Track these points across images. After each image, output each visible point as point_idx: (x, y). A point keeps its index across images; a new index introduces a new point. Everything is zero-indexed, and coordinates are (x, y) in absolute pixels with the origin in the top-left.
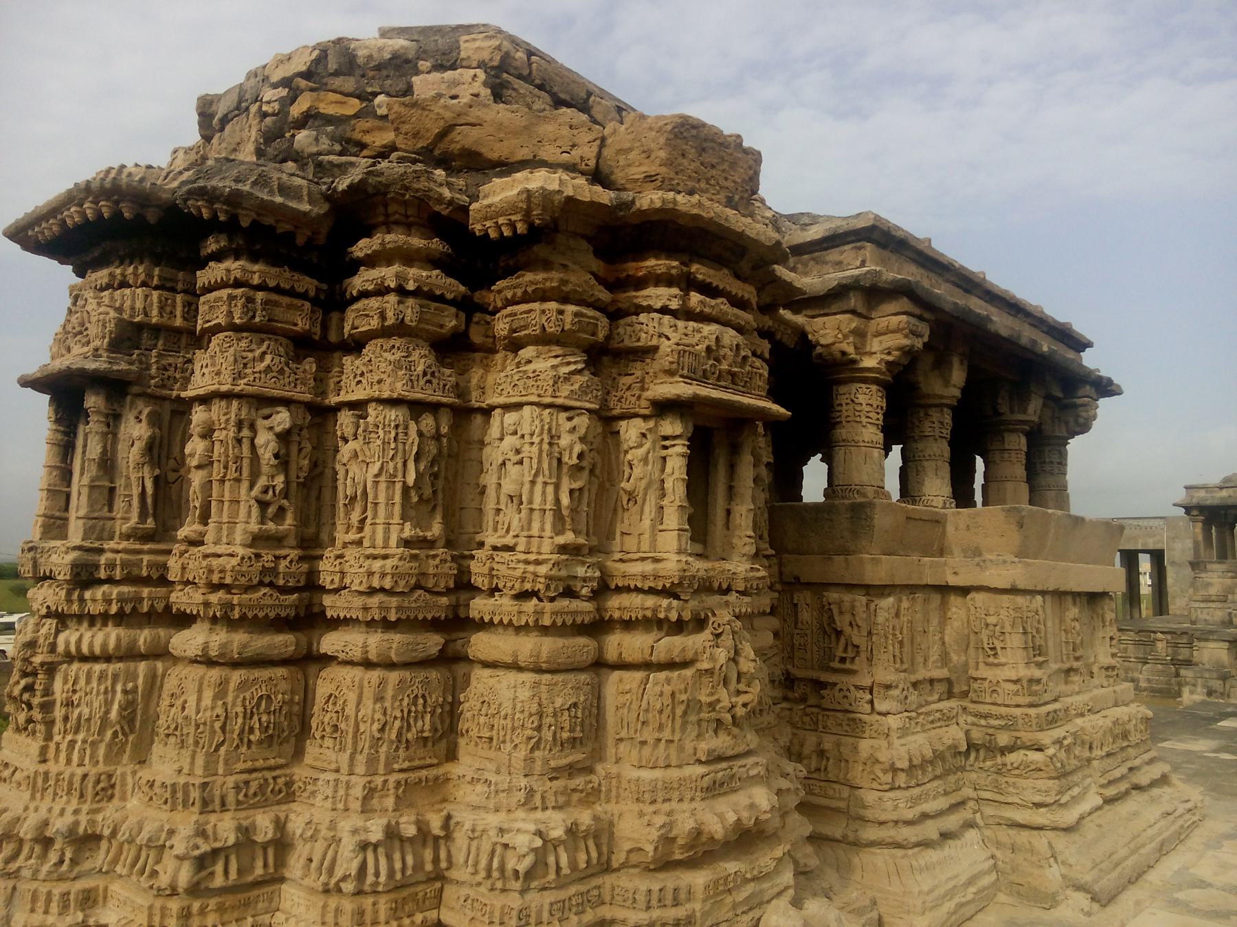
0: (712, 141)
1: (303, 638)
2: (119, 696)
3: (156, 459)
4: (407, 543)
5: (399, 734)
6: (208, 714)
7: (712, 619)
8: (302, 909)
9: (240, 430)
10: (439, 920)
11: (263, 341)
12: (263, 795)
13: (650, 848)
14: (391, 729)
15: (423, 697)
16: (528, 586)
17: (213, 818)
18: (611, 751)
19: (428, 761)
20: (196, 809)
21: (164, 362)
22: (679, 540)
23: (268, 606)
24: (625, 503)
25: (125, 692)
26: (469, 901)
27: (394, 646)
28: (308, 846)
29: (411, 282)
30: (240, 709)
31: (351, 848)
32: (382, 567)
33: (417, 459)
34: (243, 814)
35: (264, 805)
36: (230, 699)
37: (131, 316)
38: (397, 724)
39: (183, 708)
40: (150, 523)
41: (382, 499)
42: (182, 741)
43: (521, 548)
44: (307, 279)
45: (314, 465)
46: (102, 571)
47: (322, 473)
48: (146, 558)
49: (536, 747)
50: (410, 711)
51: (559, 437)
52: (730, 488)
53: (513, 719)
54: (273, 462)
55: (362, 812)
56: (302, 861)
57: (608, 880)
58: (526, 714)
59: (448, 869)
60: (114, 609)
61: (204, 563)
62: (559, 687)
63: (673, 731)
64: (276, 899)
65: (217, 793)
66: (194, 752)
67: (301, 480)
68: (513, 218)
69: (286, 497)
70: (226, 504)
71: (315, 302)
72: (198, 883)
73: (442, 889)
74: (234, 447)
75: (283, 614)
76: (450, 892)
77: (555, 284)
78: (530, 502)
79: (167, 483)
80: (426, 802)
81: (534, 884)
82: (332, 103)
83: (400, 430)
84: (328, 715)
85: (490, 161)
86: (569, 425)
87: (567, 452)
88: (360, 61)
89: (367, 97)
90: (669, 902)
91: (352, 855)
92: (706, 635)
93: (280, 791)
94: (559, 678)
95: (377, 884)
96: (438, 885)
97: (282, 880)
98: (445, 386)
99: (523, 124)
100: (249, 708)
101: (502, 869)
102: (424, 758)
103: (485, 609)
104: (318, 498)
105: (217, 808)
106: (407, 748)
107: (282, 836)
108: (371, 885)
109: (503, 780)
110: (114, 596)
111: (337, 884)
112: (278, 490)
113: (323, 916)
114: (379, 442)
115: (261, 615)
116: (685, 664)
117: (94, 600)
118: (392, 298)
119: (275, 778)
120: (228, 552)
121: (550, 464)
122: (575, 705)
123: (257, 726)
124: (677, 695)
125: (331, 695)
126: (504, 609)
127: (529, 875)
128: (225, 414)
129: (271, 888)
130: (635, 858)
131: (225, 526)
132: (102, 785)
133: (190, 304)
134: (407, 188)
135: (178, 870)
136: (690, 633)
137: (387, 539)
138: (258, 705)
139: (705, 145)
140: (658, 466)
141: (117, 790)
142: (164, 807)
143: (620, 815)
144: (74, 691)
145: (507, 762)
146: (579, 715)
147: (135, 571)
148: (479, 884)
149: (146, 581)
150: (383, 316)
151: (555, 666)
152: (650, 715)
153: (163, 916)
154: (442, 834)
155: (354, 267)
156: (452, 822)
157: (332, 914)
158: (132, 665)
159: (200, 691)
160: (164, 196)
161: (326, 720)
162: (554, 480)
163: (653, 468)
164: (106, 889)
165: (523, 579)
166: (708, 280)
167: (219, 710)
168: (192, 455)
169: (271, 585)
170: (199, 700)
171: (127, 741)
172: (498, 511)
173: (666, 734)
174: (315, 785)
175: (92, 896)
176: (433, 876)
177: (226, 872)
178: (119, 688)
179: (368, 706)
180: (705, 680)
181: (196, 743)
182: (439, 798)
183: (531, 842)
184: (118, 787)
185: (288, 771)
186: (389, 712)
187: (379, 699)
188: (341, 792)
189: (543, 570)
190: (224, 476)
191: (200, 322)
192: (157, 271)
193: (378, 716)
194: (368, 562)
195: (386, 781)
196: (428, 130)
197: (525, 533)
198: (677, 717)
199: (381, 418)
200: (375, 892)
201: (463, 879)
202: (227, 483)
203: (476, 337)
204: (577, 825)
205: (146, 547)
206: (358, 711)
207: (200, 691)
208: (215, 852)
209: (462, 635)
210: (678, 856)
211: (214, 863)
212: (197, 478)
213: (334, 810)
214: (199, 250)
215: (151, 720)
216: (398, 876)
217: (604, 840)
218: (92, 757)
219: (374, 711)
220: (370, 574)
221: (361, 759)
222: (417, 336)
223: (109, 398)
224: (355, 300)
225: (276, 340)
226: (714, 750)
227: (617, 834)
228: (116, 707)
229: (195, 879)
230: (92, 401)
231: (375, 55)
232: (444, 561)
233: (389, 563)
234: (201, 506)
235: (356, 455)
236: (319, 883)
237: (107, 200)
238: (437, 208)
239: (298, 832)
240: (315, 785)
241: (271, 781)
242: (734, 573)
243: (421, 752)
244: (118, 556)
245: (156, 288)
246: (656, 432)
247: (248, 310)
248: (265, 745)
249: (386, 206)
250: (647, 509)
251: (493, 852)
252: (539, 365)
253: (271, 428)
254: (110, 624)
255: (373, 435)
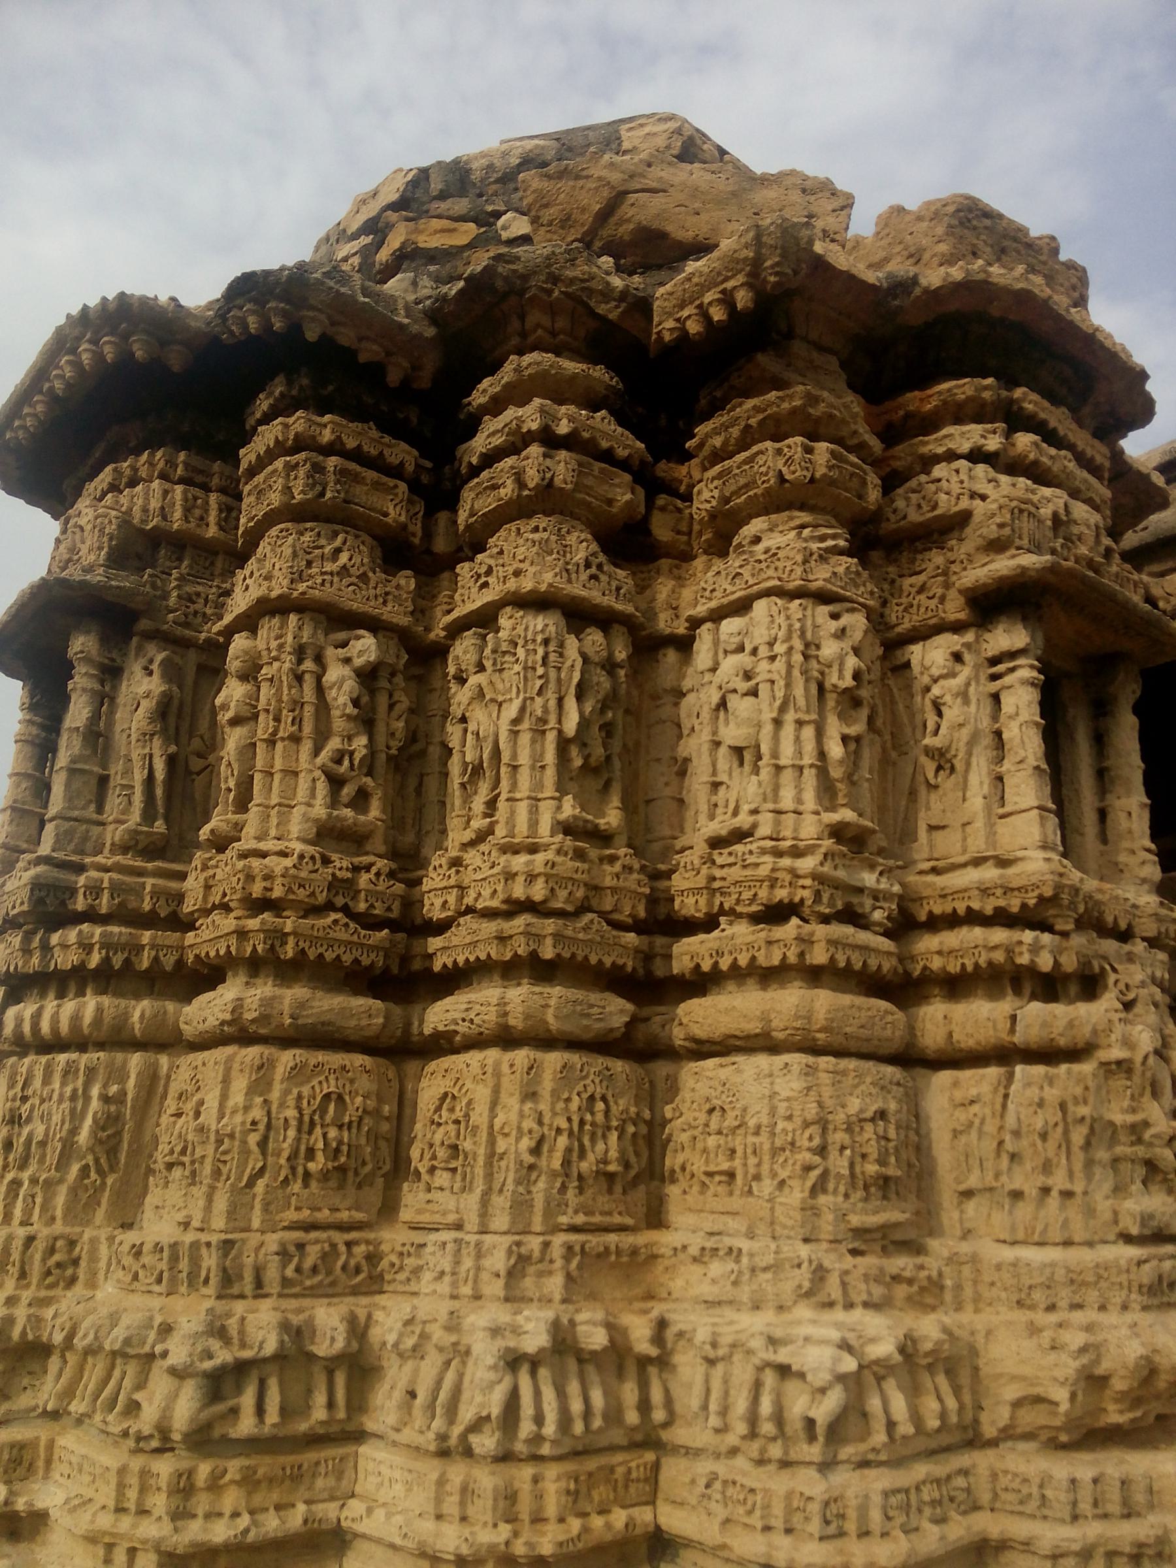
0: (1015, 240)
1: (397, 1010)
2: (95, 1104)
3: (172, 731)
4: (567, 829)
5: (566, 1163)
6: (238, 1119)
7: (1112, 977)
8: (399, 1488)
9: (300, 661)
10: (658, 1528)
11: (335, 534)
12: (329, 1273)
13: (1061, 1395)
14: (551, 1151)
15: (604, 1099)
16: (781, 894)
17: (239, 1307)
18: (950, 1216)
19: (617, 1219)
20: (211, 1290)
21: (189, 589)
22: (1042, 825)
23: (341, 942)
24: (930, 775)
25: (105, 1099)
26: (718, 1485)
27: (552, 1002)
28: (410, 1365)
29: (565, 421)
30: (291, 1113)
31: (490, 1361)
32: (528, 863)
33: (579, 697)
34: (293, 1303)
35: (328, 1292)
36: (275, 1095)
37: (142, 521)
38: (563, 1141)
39: (197, 1114)
40: (160, 826)
41: (524, 759)
42: (194, 1173)
43: (764, 830)
44: (404, 446)
45: (412, 737)
46: (81, 897)
47: (423, 753)
48: (150, 882)
49: (819, 1188)
50: (582, 1122)
51: (818, 647)
52: (1101, 774)
53: (773, 1134)
54: (350, 710)
55: (507, 1300)
56: (398, 1395)
57: (982, 1461)
58: (798, 1121)
59: (666, 1425)
60: (95, 960)
61: (240, 864)
62: (850, 1080)
63: (1071, 1175)
64: (349, 1473)
65: (249, 1261)
66: (212, 1189)
67: (394, 752)
68: (730, 284)
69: (370, 773)
70: (277, 778)
71: (415, 486)
72: (208, 1426)
73: (656, 1467)
74: (290, 687)
75: (365, 961)
76: (674, 1470)
77: (797, 403)
78: (775, 755)
79: (188, 772)
80: (618, 1295)
81: (847, 1452)
82: (436, 232)
83: (551, 648)
84: (442, 1130)
85: (680, 244)
86: (834, 625)
87: (835, 668)
88: (475, 176)
89: (487, 220)
90: (1115, 1508)
91: (492, 1376)
92: (1108, 1002)
93: (358, 1270)
94: (851, 1064)
95: (538, 1439)
96: (650, 1456)
97: (360, 1436)
98: (618, 589)
99: (730, 188)
100: (307, 1112)
101: (779, 1418)
102: (609, 1213)
103: (703, 950)
104: (419, 790)
105: (248, 1289)
106: (581, 1190)
107: (360, 1351)
108: (528, 1441)
109: (761, 1249)
110: (96, 938)
111: (463, 1437)
112: (357, 757)
113: (438, 1501)
114: (517, 668)
115: (329, 956)
116: (1075, 1054)
117: (65, 946)
118: (535, 450)
119: (349, 1245)
120: (278, 848)
121: (806, 689)
122: (882, 1114)
123: (320, 1145)
124: (1071, 1108)
125: (446, 1095)
126: (738, 941)
127: (836, 1431)
128: (277, 638)
129: (340, 1451)
130: (1030, 1418)
131: (274, 812)
132: (57, 1257)
133: (230, 509)
134: (555, 279)
135: (174, 1396)
136: (1071, 1002)
137: (534, 824)
138: (323, 1109)
139: (1006, 243)
140: (987, 707)
141: (82, 1272)
142: (156, 1288)
143: (989, 1333)
144: (24, 1099)
145: (766, 1213)
146: (892, 1134)
147: (133, 904)
148: (734, 1452)
149: (149, 921)
150: (521, 483)
151: (840, 1039)
152: (1025, 1142)
153: (143, 1490)
154: (654, 1352)
155: (471, 428)
156: (670, 1334)
157: (456, 1498)
158: (119, 1056)
159: (226, 1081)
160: (193, 324)
161: (438, 1137)
162: (814, 717)
163: (978, 713)
164: (51, 1445)
165: (773, 883)
166: (1042, 415)
167: (257, 1113)
168: (225, 707)
169: (346, 910)
170: (224, 1097)
171: (104, 1184)
172: (716, 786)
173: (1059, 1181)
174: (419, 1256)
175: (27, 1457)
176: (639, 1437)
177: (260, 1411)
178: (95, 1092)
179: (511, 1109)
180: (1120, 1082)
181: (217, 1173)
182: (639, 1291)
183: (836, 1360)
184: (83, 1263)
185: (371, 1236)
186: (546, 1120)
187: (530, 1095)
188: (468, 1263)
189: (807, 864)
190: (275, 733)
191: (243, 521)
192: (182, 456)
193: (528, 1124)
194: (503, 859)
195: (546, 1245)
196: (584, 210)
197: (771, 806)
198: (1075, 1149)
199: (520, 630)
200: (536, 1458)
201: (698, 1444)
202: (279, 746)
203: (662, 529)
204: (914, 1342)
205: (150, 865)
206: (493, 1115)
207: (226, 1081)
208: (241, 1368)
209: (662, 1009)
210: (1115, 1416)
211: (239, 1390)
212: (233, 739)
213: (454, 1297)
214: (243, 422)
215: (142, 1150)
216: (578, 1428)
217: (965, 1379)
218: (45, 1208)
219: (521, 1115)
220: (510, 876)
221: (501, 1202)
222: (573, 516)
223: (105, 641)
224: (475, 471)
225: (357, 537)
226: (1151, 1216)
227: (985, 1370)
228: (89, 1121)
229: (205, 1415)
230: (82, 644)
231: (497, 163)
232: (628, 869)
233: (540, 858)
234: (237, 785)
235: (481, 694)
236: (431, 1435)
237: (112, 334)
238: (602, 309)
239: (391, 1338)
240: (419, 1256)
241: (342, 1248)
242: (1134, 906)
243: (603, 1201)
244: (106, 876)
245: (181, 481)
246: (977, 652)
247: (314, 485)
248: (333, 1183)
249: (522, 318)
250: (974, 779)
251: (758, 1386)
252: (771, 541)
253: (347, 661)
254: (89, 991)
255: (507, 658)
